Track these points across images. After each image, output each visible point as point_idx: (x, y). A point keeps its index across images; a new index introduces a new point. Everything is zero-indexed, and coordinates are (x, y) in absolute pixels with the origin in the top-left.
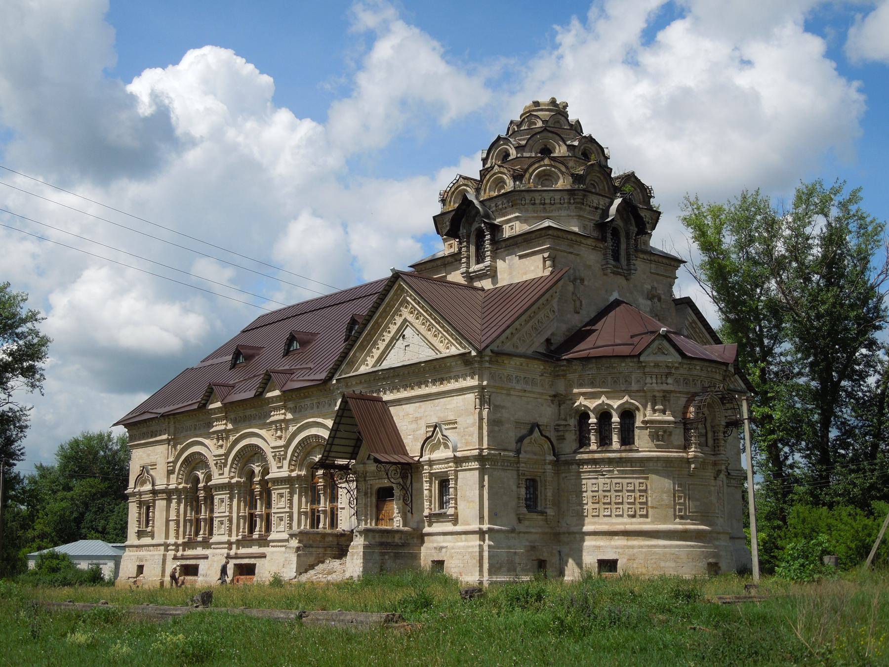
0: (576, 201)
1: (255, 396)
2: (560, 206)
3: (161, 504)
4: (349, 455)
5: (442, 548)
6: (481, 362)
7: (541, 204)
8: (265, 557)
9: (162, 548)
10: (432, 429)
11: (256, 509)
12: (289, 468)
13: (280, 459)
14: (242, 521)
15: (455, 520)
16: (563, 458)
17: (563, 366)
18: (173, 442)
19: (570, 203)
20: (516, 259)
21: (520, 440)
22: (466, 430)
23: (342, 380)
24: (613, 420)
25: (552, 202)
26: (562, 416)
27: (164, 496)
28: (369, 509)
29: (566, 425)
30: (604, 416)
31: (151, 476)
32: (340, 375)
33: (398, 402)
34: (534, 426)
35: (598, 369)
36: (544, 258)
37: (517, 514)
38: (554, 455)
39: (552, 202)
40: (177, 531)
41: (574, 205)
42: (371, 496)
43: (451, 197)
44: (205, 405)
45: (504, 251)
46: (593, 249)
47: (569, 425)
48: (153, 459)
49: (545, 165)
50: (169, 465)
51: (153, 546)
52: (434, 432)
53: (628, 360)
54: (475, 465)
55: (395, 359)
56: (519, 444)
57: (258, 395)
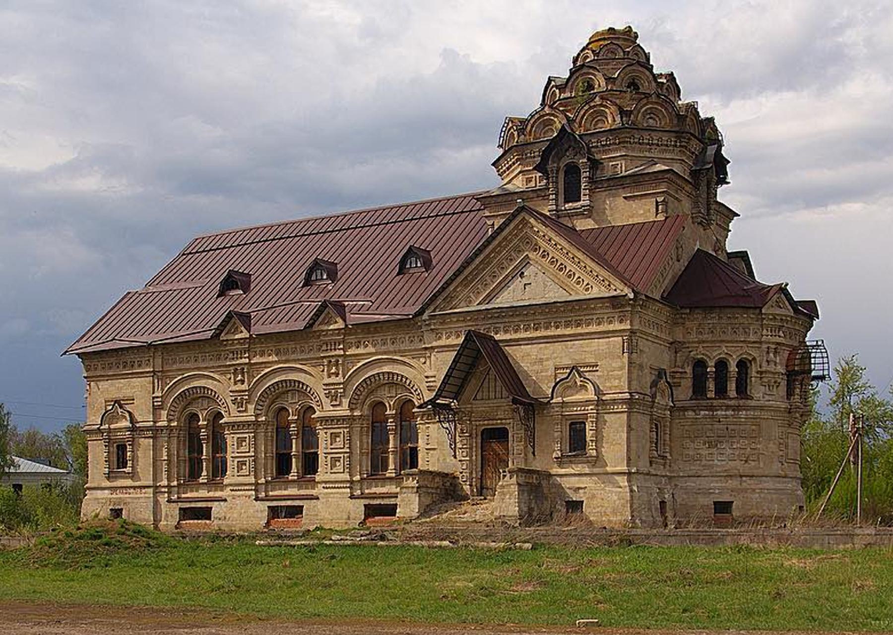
0: (621, 140)
1: (305, 327)
2: (667, 148)
3: (146, 443)
4: (453, 395)
5: (579, 488)
6: (633, 306)
7: (648, 144)
8: (318, 498)
9: (151, 490)
10: (568, 371)
11: (291, 449)
12: (349, 407)
13: (333, 397)
14: (269, 462)
15: (133, 475)
16: (678, 404)
17: (685, 314)
18: (159, 375)
19: (676, 146)
20: (620, 201)
21: (654, 384)
22: (611, 373)
23: (438, 317)
24: (732, 369)
25: (660, 143)
26: (679, 363)
27: (150, 434)
28: (474, 449)
29: (681, 373)
30: (722, 365)
31: (128, 412)
32: (434, 311)
33: (517, 342)
34: (661, 373)
35: (720, 318)
36: (657, 202)
37: (650, 457)
38: (673, 402)
39: (660, 143)
40: (169, 471)
41: (679, 149)
42: (476, 438)
43: (532, 127)
44: (218, 335)
45: (605, 191)
46: (688, 196)
47: (686, 372)
48: (127, 392)
49: (652, 103)
50: (156, 400)
51: (134, 488)
52: (570, 374)
53: (751, 311)
54: (624, 408)
55: (505, 300)
56: (654, 389)
57: (308, 327)
